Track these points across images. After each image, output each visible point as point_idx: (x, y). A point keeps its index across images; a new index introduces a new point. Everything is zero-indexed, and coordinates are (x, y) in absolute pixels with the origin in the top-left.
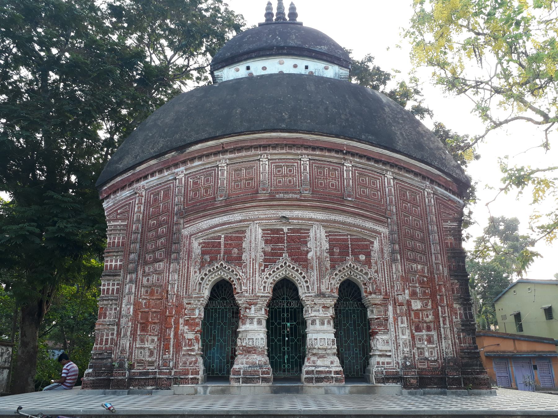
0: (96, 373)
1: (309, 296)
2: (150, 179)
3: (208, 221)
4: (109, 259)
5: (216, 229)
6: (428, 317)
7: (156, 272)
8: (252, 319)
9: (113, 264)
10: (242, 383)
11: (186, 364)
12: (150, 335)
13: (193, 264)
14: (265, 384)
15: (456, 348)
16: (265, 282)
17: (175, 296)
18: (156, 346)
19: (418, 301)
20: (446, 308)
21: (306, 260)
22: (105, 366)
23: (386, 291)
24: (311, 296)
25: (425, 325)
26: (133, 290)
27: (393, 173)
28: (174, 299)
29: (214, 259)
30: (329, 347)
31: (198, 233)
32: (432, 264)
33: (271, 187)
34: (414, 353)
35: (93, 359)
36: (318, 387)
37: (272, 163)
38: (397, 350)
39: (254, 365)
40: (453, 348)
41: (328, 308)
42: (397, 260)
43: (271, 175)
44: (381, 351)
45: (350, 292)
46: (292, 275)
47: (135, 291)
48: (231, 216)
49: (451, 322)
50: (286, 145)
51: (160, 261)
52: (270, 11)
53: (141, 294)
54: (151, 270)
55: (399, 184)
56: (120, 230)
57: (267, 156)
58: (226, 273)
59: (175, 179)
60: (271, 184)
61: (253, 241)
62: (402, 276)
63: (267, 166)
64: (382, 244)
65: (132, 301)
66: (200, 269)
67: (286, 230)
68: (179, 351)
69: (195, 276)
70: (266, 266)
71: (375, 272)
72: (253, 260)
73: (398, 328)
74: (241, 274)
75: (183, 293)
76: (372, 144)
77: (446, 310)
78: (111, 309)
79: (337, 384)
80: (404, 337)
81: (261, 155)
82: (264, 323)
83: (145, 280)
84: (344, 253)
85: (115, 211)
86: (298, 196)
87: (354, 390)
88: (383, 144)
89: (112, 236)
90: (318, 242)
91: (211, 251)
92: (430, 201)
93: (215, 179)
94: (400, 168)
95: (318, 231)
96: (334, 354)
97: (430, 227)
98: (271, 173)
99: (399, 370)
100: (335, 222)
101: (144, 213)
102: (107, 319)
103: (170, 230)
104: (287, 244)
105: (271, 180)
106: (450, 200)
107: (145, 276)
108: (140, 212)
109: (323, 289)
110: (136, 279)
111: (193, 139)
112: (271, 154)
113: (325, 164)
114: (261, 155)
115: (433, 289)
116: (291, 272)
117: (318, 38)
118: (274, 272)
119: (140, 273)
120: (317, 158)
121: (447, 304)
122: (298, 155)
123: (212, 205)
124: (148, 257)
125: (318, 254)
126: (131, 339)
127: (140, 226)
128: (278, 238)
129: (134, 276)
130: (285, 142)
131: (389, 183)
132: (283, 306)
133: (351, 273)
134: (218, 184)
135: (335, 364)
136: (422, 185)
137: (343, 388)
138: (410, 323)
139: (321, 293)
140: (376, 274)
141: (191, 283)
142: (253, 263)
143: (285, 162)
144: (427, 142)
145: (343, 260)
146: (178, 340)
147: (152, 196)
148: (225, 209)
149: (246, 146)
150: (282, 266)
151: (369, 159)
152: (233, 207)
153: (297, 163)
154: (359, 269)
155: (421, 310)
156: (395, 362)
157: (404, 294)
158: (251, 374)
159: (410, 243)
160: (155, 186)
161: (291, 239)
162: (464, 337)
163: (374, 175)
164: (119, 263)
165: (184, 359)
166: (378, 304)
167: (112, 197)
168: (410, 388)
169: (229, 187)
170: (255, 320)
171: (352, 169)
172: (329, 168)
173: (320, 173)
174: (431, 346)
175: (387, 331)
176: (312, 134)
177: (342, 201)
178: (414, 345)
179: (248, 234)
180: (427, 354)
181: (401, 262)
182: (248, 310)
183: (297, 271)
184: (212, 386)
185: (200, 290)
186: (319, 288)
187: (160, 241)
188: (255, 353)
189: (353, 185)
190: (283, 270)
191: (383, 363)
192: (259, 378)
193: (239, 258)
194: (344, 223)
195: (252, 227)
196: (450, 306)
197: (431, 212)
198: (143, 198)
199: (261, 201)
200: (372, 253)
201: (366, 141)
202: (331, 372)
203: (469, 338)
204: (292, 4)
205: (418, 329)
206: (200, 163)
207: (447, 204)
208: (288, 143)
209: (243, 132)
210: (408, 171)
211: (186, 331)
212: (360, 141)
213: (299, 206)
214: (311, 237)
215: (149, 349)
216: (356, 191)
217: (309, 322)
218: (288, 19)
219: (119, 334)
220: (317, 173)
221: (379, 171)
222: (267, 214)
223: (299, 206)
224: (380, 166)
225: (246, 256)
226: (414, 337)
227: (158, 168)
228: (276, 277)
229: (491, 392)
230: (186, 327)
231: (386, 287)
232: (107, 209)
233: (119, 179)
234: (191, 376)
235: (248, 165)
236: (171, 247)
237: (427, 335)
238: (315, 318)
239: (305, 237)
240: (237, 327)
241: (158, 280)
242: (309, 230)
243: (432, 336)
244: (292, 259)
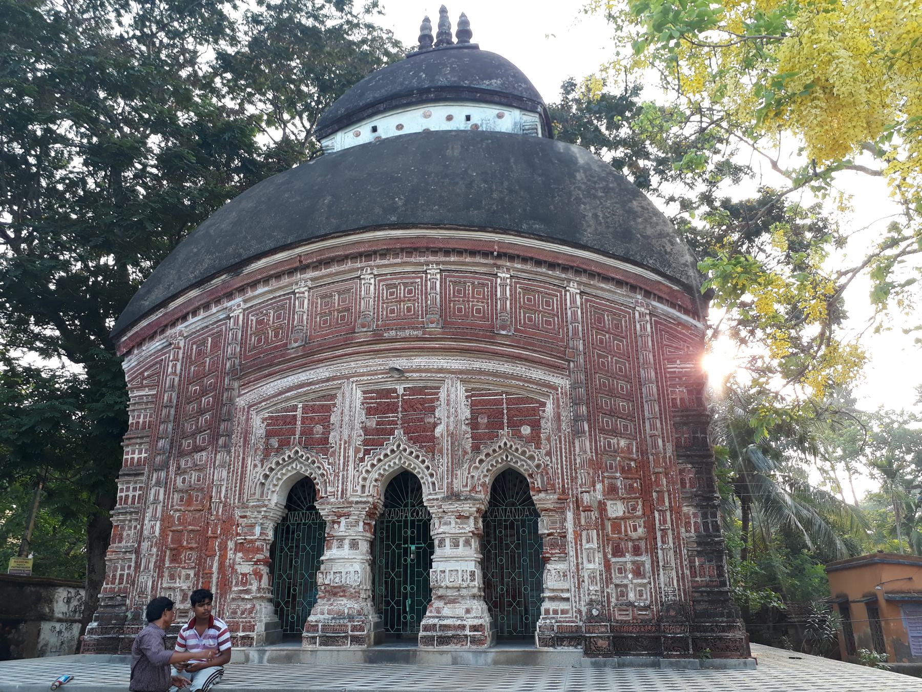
0: (103, 629)
1: (433, 499)
2: (191, 320)
3: (275, 383)
4: (129, 449)
5: (289, 394)
6: (635, 530)
7: (200, 469)
8: (341, 540)
9: (136, 456)
10: (320, 645)
11: (236, 613)
12: (184, 568)
13: (252, 452)
14: (356, 647)
15: (684, 585)
16: (365, 479)
17: (221, 505)
18: (191, 585)
19: (619, 503)
20: (668, 513)
21: (433, 439)
22: (116, 617)
23: (563, 486)
24: (437, 499)
25: (630, 544)
26: (161, 497)
27: (579, 283)
28: (220, 511)
29: (285, 444)
30: (465, 585)
31: (260, 403)
32: (645, 437)
33: (378, 320)
34: (608, 593)
35: (101, 606)
37: (380, 281)
38: (579, 588)
39: (340, 615)
40: (679, 585)
41: (468, 518)
42: (584, 432)
43: (379, 300)
44: (553, 590)
45: (509, 489)
46: (410, 465)
47: (164, 499)
48: (312, 372)
49: (677, 538)
50: (402, 250)
51: (202, 450)
52: (426, 32)
53: (172, 502)
54: (190, 464)
55: (591, 301)
56: (147, 403)
57: (372, 269)
58: (305, 465)
59: (229, 318)
60: (378, 316)
61: (346, 411)
62: (591, 460)
63: (372, 287)
64: (558, 406)
65: (159, 514)
66: (262, 461)
67: (401, 391)
68: (226, 593)
69: (255, 472)
70: (367, 452)
71: (546, 455)
72: (345, 443)
73: (582, 550)
74: (326, 466)
75: (234, 500)
76: (540, 238)
77: (668, 518)
78: (130, 528)
79: (474, 647)
80: (591, 566)
81: (362, 269)
82: (364, 546)
83: (179, 480)
84: (495, 424)
85: (140, 374)
86: (419, 333)
87: (502, 657)
88: (559, 236)
89: (136, 413)
90: (453, 408)
91: (280, 430)
92: (643, 328)
93: (289, 314)
94: (592, 275)
95: (453, 389)
96: (474, 597)
97: (642, 372)
98: (379, 297)
99: (581, 624)
100: (481, 372)
101: (181, 374)
102: (124, 543)
103: (218, 401)
104: (403, 413)
105: (378, 309)
106: (679, 324)
107: (180, 475)
108: (174, 373)
109: (457, 486)
110: (167, 479)
111: (252, 252)
112: (378, 267)
113: (466, 277)
114: (362, 269)
115: (645, 482)
116: (409, 460)
117: (496, 66)
118: (380, 460)
119: (172, 469)
120: (453, 267)
121: (670, 507)
122: (421, 264)
123: (282, 356)
124: (185, 443)
125: (451, 428)
126: (156, 575)
127: (174, 395)
128: (388, 404)
129: (163, 474)
130: (398, 246)
131: (573, 301)
132: (406, 517)
133: (507, 457)
134: (293, 321)
135: (473, 614)
136: (630, 301)
137: (483, 655)
138: (603, 541)
139: (452, 494)
140: (548, 458)
141: (247, 484)
142: (345, 449)
143: (402, 278)
144: (641, 227)
145: (493, 437)
146: (224, 575)
147: (194, 347)
148: (304, 361)
149: (336, 256)
150: (393, 451)
151: (539, 263)
152: (316, 357)
153: (421, 278)
154: (520, 451)
155: (622, 518)
156: (574, 609)
157: (595, 490)
158: (334, 631)
159: (605, 402)
160: (198, 331)
161: (409, 405)
162: (701, 566)
163: (548, 289)
164: (143, 455)
165: (233, 607)
166: (551, 510)
167: (136, 352)
168: (597, 655)
169: (311, 325)
170: (347, 542)
171: (511, 282)
172: (473, 283)
173: (459, 292)
174: (639, 581)
175: (564, 557)
176: (441, 228)
177: (492, 337)
178: (609, 580)
179: (338, 401)
180: (632, 596)
181: (590, 435)
182: (336, 526)
183: (417, 457)
184: (271, 650)
185: (262, 495)
186: (450, 486)
187: (205, 419)
189: (511, 308)
190: (395, 458)
191: (555, 612)
192: (346, 637)
193: (325, 441)
194: (495, 374)
195: (346, 388)
196: (675, 511)
197: (645, 346)
198: (181, 352)
199: (361, 344)
200: (543, 422)
201: (530, 234)
202: (463, 627)
203: (710, 568)
204: (463, 15)
206: (266, 289)
207: (676, 330)
208: (404, 246)
209: (330, 234)
210: (606, 279)
211: (238, 560)
212: (519, 234)
213: (422, 349)
214: (442, 399)
215: (182, 590)
216: (516, 318)
217: (436, 542)
218: (455, 40)
219: (138, 566)
220: (454, 292)
221: (556, 282)
222: (371, 366)
223: (422, 349)
224: (557, 273)
225: (335, 437)
226: (610, 565)
227: (202, 302)
228: (385, 470)
229: (745, 664)
230: (240, 555)
231: (563, 480)
232: (128, 371)
233: (144, 323)
234: (241, 634)
235: (343, 286)
236: (218, 427)
237: (633, 563)
238: (443, 536)
239: (432, 401)
240: (321, 553)
241: (199, 480)
242: (439, 388)
243: (643, 563)
244: (410, 439)
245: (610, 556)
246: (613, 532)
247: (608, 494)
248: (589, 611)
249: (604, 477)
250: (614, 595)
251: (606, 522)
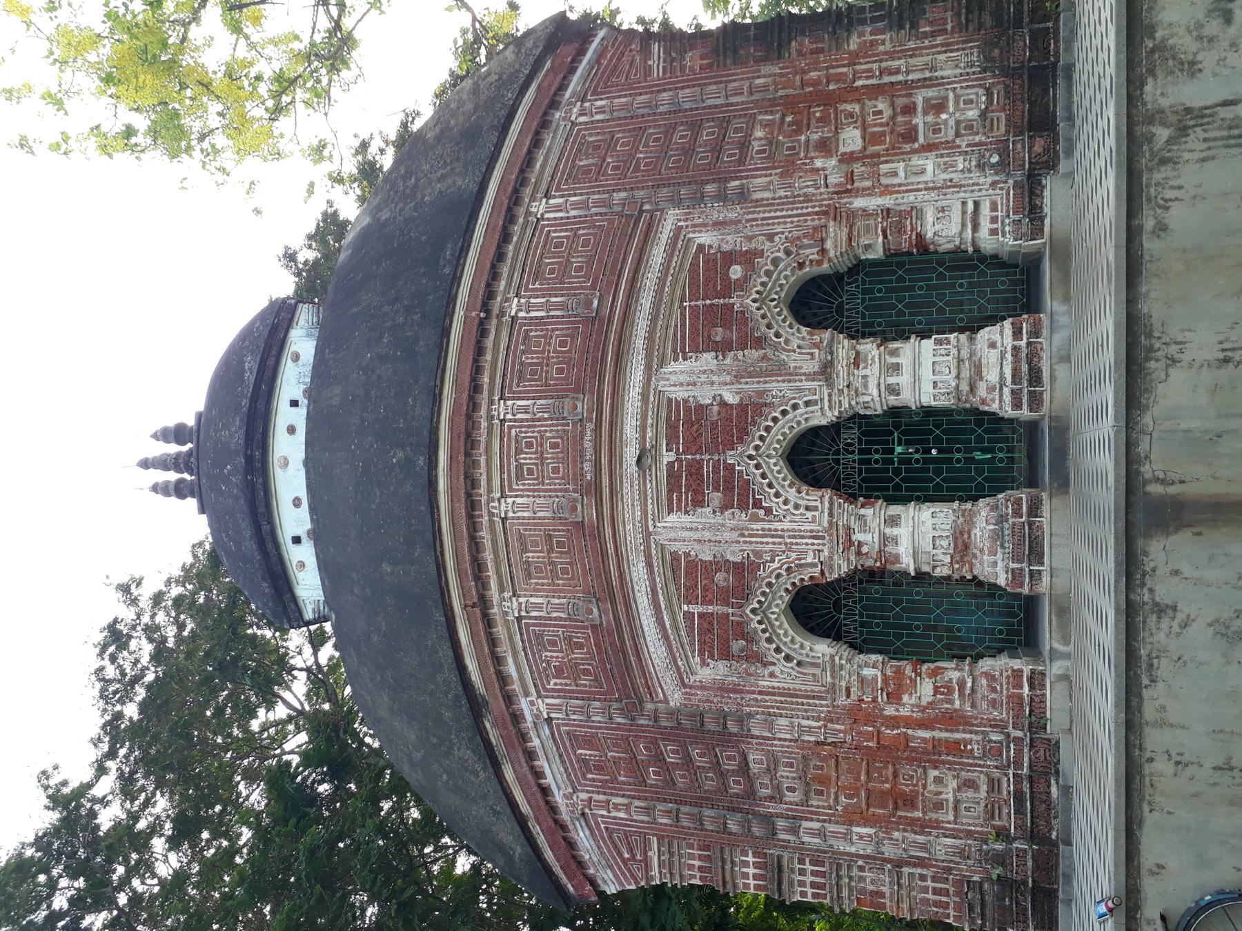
30: (954, 351)
36: (1053, 378)
38: (961, 186)
99: (1011, 182)
135: (997, 338)
138: (896, 154)
140: (777, 238)
145: (743, 318)
155: (864, 130)
175: (916, 212)
178: (950, 145)
202: (1016, 350)
250: (971, 138)
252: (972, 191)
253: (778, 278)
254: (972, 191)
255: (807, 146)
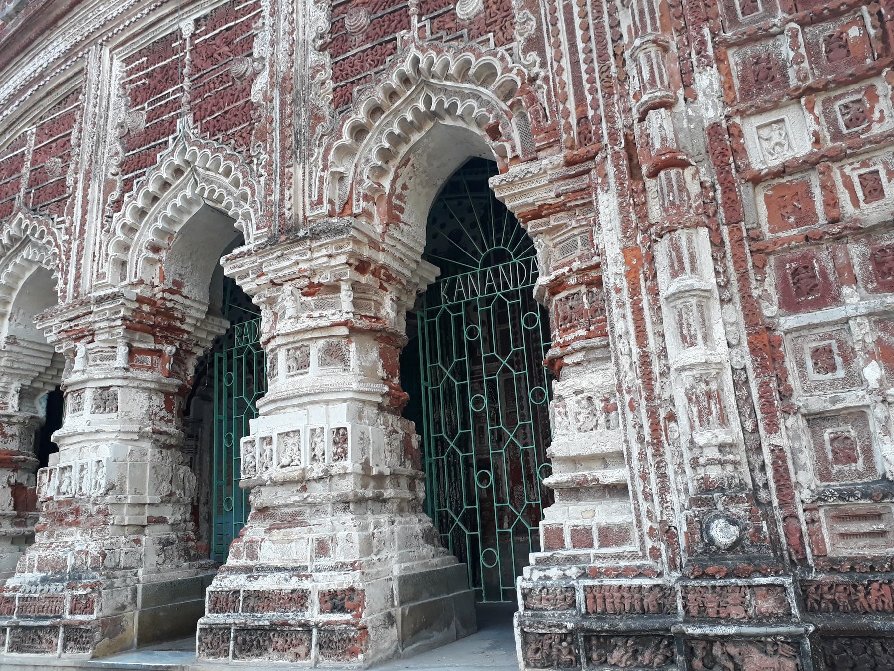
30: (317, 470)
34: (778, 451)
38: (657, 444)
41: (334, 288)
80: (696, 354)
99: (671, 579)
135: (338, 555)
138: (739, 261)
140: (534, 56)
145: (383, 48)
155: (809, 164)
157: (691, 97)
175: (600, 351)
178: (776, 402)
183: (228, 173)
188: (77, 524)
191: (582, 537)
192: (54, 629)
202: (300, 599)
205: (805, 288)
245: (770, 310)
246: (778, 219)
247: (746, 94)
248: (700, 527)
249: (722, 45)
250: (807, 458)
251: (744, 191)
252: (644, 477)
253: (464, 96)
254: (644, 477)
255: (753, 39)
